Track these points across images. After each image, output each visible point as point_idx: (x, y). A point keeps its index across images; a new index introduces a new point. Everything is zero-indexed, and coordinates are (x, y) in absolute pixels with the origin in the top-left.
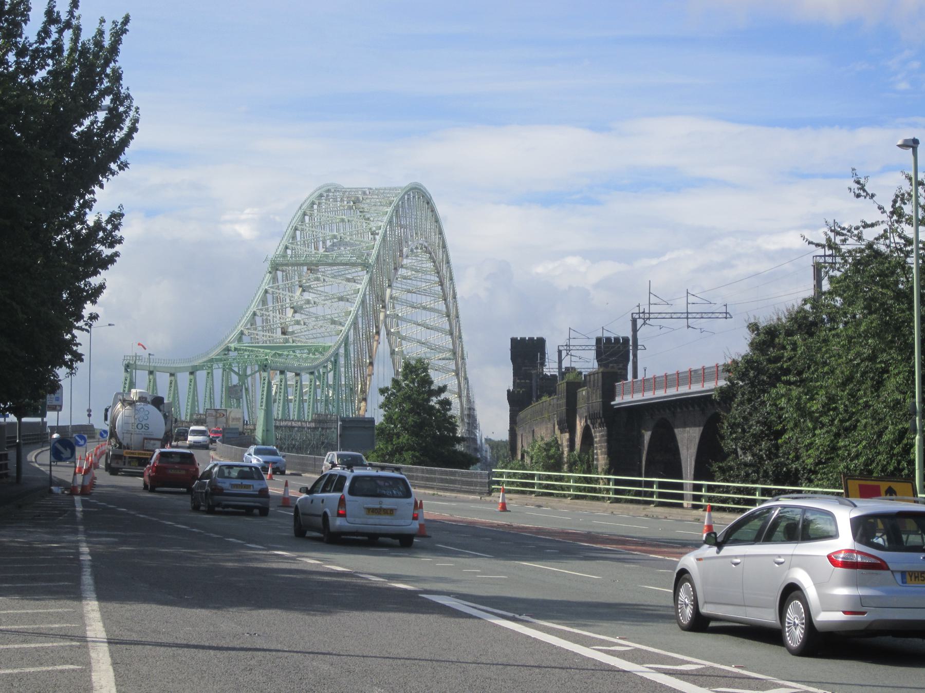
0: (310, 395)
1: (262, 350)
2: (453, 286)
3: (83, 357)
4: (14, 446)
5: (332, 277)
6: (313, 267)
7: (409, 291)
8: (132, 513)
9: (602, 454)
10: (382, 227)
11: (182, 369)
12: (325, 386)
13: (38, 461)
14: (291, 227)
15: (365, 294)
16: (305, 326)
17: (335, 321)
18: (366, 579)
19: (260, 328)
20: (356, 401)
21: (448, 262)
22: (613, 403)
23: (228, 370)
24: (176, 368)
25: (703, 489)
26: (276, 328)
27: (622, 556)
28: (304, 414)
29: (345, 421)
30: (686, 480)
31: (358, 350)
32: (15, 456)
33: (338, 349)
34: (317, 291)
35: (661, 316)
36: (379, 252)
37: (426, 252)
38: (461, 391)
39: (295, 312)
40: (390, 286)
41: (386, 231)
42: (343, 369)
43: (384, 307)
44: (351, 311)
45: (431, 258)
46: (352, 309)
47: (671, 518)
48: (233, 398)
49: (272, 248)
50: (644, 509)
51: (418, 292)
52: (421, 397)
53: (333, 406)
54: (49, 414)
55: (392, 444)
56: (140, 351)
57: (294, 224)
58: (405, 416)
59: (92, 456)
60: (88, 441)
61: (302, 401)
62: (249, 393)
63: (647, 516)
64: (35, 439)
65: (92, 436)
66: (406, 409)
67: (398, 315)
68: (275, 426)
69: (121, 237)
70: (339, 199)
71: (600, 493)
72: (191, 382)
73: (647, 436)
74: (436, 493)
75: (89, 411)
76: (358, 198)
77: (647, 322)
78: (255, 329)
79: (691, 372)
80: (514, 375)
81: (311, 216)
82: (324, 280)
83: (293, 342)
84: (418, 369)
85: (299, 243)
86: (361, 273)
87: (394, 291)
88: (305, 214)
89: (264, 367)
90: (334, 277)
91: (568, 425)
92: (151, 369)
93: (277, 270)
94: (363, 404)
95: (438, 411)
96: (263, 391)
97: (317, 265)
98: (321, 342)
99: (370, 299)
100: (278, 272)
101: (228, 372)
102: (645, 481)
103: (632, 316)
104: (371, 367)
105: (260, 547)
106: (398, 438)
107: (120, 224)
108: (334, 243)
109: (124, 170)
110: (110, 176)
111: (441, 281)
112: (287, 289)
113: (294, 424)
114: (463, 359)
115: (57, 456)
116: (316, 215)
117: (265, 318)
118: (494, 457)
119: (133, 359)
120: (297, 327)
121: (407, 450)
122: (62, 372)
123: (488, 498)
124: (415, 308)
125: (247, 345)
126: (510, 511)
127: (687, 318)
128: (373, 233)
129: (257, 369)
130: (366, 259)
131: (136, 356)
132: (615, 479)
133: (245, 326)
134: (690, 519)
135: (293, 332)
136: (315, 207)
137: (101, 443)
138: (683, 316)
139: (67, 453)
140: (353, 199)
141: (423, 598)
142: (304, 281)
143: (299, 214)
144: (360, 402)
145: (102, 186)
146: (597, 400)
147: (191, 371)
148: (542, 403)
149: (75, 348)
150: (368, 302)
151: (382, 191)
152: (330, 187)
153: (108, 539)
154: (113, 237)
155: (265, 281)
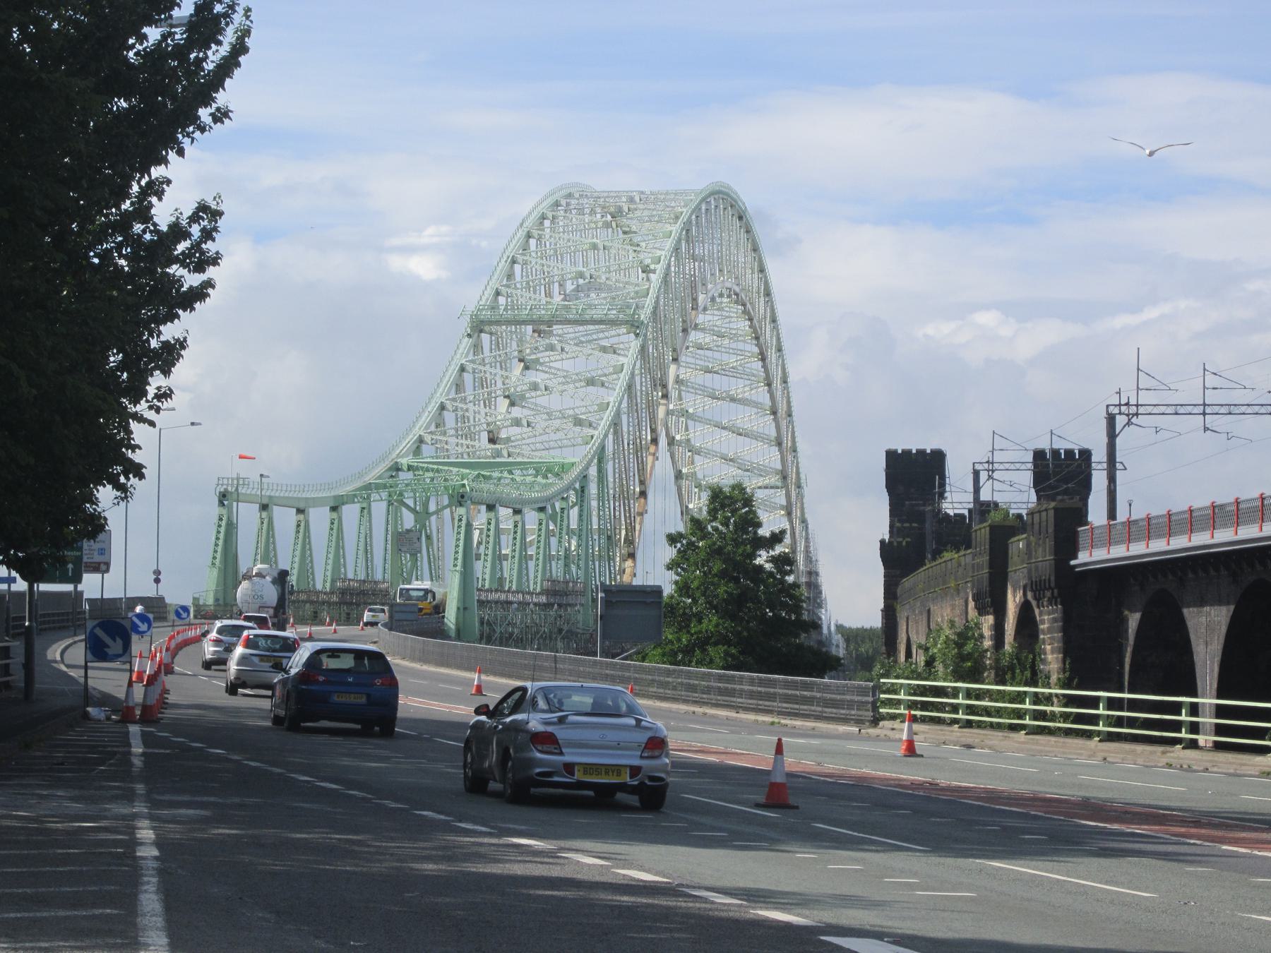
0: (538, 548)
1: (455, 470)
2: (783, 361)
3: (144, 470)
4: (19, 634)
5: (576, 345)
6: (542, 326)
7: (708, 371)
8: (236, 757)
9: (1052, 653)
10: (662, 258)
11: (317, 502)
12: (564, 532)
13: (66, 662)
14: (505, 259)
15: (633, 374)
16: (530, 429)
17: (580, 419)
18: (705, 900)
19: (452, 432)
20: (618, 559)
21: (774, 320)
22: (1073, 562)
23: (396, 503)
24: (307, 499)
25: (1184, 711)
26: (480, 432)
27: (1170, 848)
28: (528, 580)
29: (611, 591)
30: (1203, 697)
31: (620, 471)
32: (23, 651)
33: (587, 468)
34: (550, 367)
35: (1159, 410)
36: (657, 302)
37: (736, 302)
38: (795, 543)
39: (512, 404)
40: (675, 360)
41: (669, 265)
42: (594, 504)
43: (665, 396)
44: (608, 404)
45: (745, 312)
46: (612, 399)
47: (1215, 769)
48: (405, 552)
49: (473, 297)
50: (1164, 753)
51: (724, 371)
52: (740, 551)
53: (578, 567)
54: (87, 577)
55: (688, 632)
57: (510, 252)
58: (713, 584)
59: (161, 652)
60: (154, 625)
61: (525, 558)
62: (432, 544)
63: (1170, 766)
64: (63, 621)
65: (162, 617)
66: (715, 570)
67: (687, 411)
68: (478, 601)
69: (217, 253)
70: (587, 211)
71: (1054, 721)
72: (332, 523)
73: (1133, 620)
74: (776, 720)
75: (157, 572)
76: (620, 210)
77: (1134, 420)
78: (444, 433)
79: (1214, 507)
80: (891, 516)
81: (539, 238)
82: (562, 349)
83: (509, 456)
84: (736, 502)
85: (519, 286)
86: (624, 338)
87: (682, 370)
88: (529, 236)
89: (460, 499)
90: (579, 343)
91: (993, 601)
92: (265, 501)
93: (481, 331)
94: (629, 563)
95: (771, 574)
96: (458, 540)
97: (550, 323)
98: (555, 457)
99: (641, 383)
100: (483, 335)
101: (396, 507)
102: (1129, 700)
103: (1107, 411)
104: (642, 500)
105: (484, 829)
106: (700, 622)
107: (215, 229)
108: (578, 286)
109: (223, 123)
110: (197, 134)
111: (762, 353)
112: (498, 364)
113: (511, 597)
114: (799, 486)
115: (98, 651)
116: (548, 237)
117: (460, 413)
118: (851, 656)
119: (232, 484)
120: (514, 431)
121: (716, 644)
122: (105, 494)
123: (873, 731)
124: (717, 399)
125: (429, 460)
126: (922, 756)
127: (1204, 414)
128: (646, 270)
129: (446, 502)
130: (634, 314)
131: (238, 479)
132: (1064, 695)
133: (427, 428)
134: (1253, 773)
135: (508, 440)
136: (547, 223)
137: (177, 629)
138: (1196, 410)
139: (115, 646)
140: (612, 209)
141: (830, 944)
142: (528, 351)
143: (519, 235)
144: (623, 560)
145: (181, 153)
146: (1045, 557)
147: (332, 505)
148: (945, 562)
149: (130, 454)
150: (639, 388)
151: (662, 197)
152: (572, 190)
153: (191, 812)
154: (203, 253)
155: (460, 351)
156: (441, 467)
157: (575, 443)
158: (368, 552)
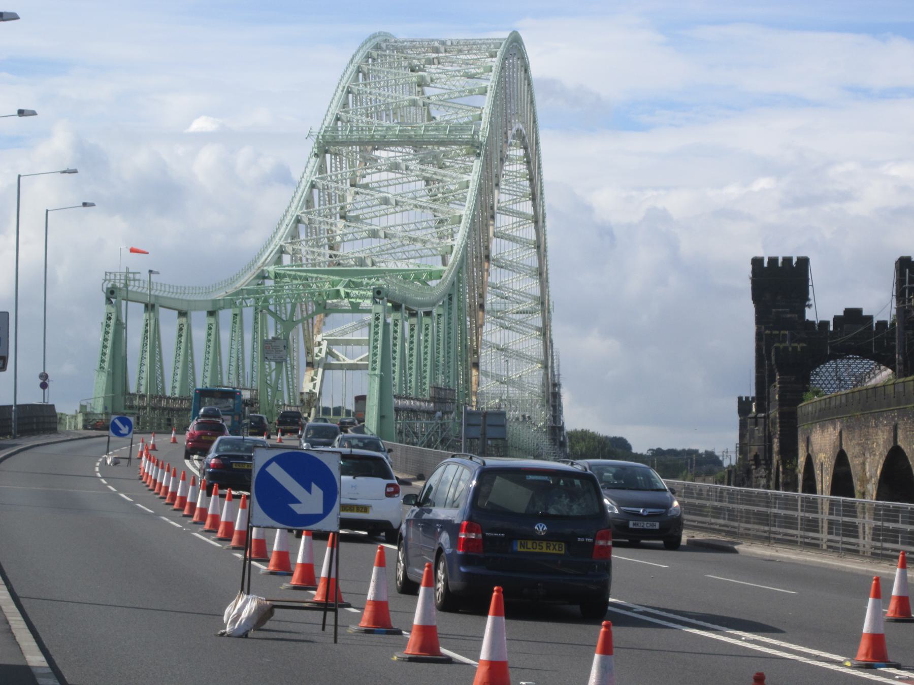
10: (489, 89)
11: (197, 306)
14: (341, 88)
23: (261, 310)
56: (138, 264)
83: (373, 264)
93: (326, 152)
131: (128, 272)
143: (350, 70)
156: (310, 275)
157: (422, 255)
158: (240, 359)
